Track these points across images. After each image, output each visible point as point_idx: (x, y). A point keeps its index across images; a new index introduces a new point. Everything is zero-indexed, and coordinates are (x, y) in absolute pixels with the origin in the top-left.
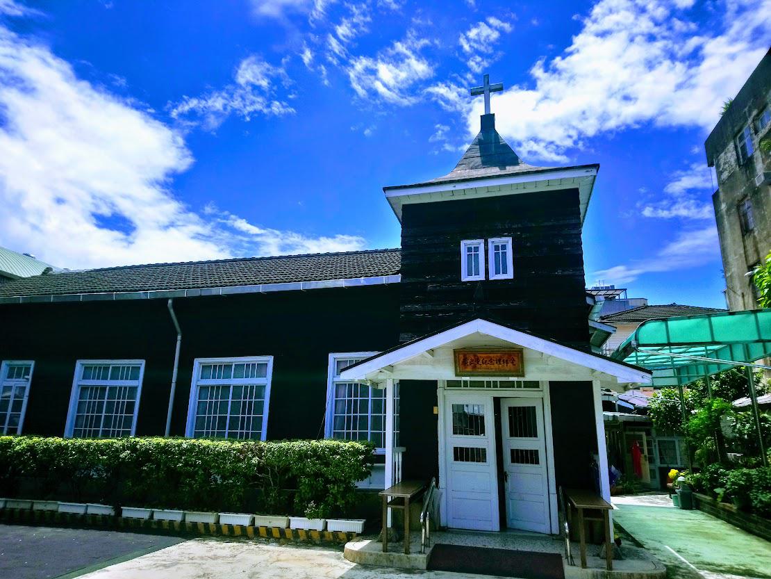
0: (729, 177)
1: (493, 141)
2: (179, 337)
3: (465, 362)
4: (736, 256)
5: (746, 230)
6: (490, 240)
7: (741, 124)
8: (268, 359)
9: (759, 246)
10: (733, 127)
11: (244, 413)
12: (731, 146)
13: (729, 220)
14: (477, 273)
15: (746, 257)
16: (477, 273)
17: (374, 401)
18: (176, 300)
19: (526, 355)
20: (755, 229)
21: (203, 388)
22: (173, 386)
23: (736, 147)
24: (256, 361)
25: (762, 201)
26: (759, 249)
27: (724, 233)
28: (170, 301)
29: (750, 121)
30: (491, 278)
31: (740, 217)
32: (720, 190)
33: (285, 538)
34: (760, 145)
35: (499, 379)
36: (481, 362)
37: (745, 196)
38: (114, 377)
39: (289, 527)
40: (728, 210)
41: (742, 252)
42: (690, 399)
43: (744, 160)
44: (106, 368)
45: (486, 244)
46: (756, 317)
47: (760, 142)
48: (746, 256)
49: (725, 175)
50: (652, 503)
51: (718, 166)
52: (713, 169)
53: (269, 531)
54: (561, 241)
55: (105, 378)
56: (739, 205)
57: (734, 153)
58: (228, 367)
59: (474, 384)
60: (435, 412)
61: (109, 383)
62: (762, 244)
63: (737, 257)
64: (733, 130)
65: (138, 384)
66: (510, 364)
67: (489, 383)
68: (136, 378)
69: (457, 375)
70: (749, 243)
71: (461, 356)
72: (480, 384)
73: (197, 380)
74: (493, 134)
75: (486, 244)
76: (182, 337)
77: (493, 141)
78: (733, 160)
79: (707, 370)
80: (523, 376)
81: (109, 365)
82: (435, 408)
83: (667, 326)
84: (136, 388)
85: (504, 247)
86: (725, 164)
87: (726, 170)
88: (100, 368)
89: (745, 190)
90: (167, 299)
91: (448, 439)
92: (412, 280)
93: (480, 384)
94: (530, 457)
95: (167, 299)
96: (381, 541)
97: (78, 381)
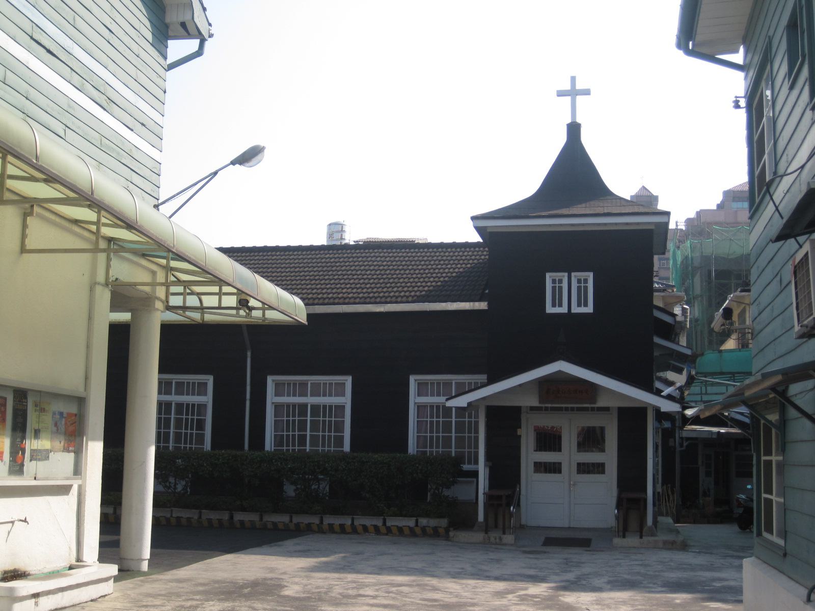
2: (249, 354)
6: (573, 274)
8: (208, 378)
14: (560, 305)
16: (560, 305)
17: (170, 414)
24: (328, 380)
30: (573, 311)
33: (391, 533)
35: (549, 405)
38: (179, 392)
39: (171, 516)
53: (400, 530)
58: (304, 385)
59: (553, 409)
61: (311, 400)
68: (343, 394)
69: (540, 403)
72: (560, 409)
73: (271, 398)
76: (252, 354)
81: (173, 379)
85: (586, 281)
91: (529, 455)
93: (560, 409)
94: (599, 468)
97: (414, 399)
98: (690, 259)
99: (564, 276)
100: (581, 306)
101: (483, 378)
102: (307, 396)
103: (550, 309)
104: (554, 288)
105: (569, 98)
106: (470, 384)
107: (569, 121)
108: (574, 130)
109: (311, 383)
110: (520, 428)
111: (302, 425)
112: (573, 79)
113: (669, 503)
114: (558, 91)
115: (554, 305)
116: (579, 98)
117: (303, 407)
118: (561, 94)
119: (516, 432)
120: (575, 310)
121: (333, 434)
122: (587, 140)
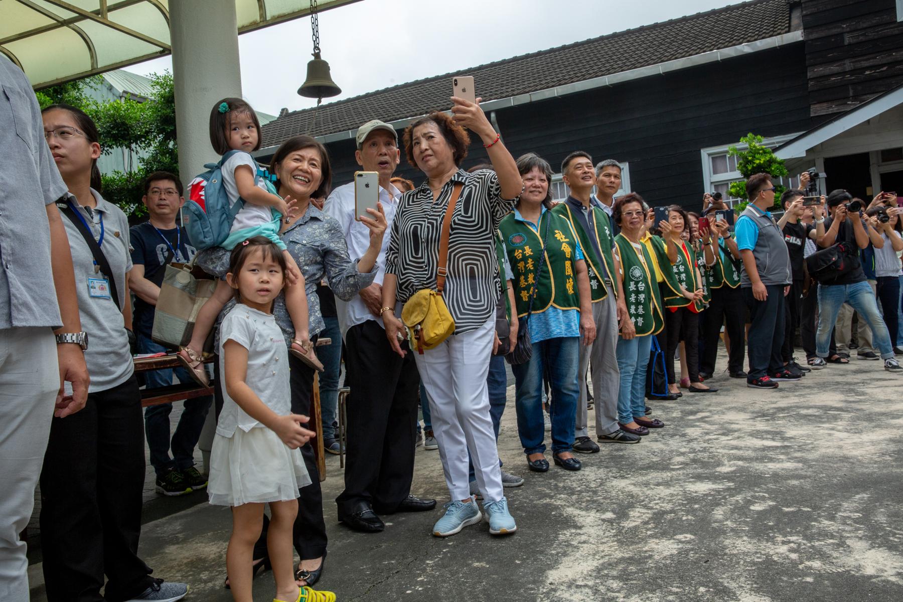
110: (871, 185)
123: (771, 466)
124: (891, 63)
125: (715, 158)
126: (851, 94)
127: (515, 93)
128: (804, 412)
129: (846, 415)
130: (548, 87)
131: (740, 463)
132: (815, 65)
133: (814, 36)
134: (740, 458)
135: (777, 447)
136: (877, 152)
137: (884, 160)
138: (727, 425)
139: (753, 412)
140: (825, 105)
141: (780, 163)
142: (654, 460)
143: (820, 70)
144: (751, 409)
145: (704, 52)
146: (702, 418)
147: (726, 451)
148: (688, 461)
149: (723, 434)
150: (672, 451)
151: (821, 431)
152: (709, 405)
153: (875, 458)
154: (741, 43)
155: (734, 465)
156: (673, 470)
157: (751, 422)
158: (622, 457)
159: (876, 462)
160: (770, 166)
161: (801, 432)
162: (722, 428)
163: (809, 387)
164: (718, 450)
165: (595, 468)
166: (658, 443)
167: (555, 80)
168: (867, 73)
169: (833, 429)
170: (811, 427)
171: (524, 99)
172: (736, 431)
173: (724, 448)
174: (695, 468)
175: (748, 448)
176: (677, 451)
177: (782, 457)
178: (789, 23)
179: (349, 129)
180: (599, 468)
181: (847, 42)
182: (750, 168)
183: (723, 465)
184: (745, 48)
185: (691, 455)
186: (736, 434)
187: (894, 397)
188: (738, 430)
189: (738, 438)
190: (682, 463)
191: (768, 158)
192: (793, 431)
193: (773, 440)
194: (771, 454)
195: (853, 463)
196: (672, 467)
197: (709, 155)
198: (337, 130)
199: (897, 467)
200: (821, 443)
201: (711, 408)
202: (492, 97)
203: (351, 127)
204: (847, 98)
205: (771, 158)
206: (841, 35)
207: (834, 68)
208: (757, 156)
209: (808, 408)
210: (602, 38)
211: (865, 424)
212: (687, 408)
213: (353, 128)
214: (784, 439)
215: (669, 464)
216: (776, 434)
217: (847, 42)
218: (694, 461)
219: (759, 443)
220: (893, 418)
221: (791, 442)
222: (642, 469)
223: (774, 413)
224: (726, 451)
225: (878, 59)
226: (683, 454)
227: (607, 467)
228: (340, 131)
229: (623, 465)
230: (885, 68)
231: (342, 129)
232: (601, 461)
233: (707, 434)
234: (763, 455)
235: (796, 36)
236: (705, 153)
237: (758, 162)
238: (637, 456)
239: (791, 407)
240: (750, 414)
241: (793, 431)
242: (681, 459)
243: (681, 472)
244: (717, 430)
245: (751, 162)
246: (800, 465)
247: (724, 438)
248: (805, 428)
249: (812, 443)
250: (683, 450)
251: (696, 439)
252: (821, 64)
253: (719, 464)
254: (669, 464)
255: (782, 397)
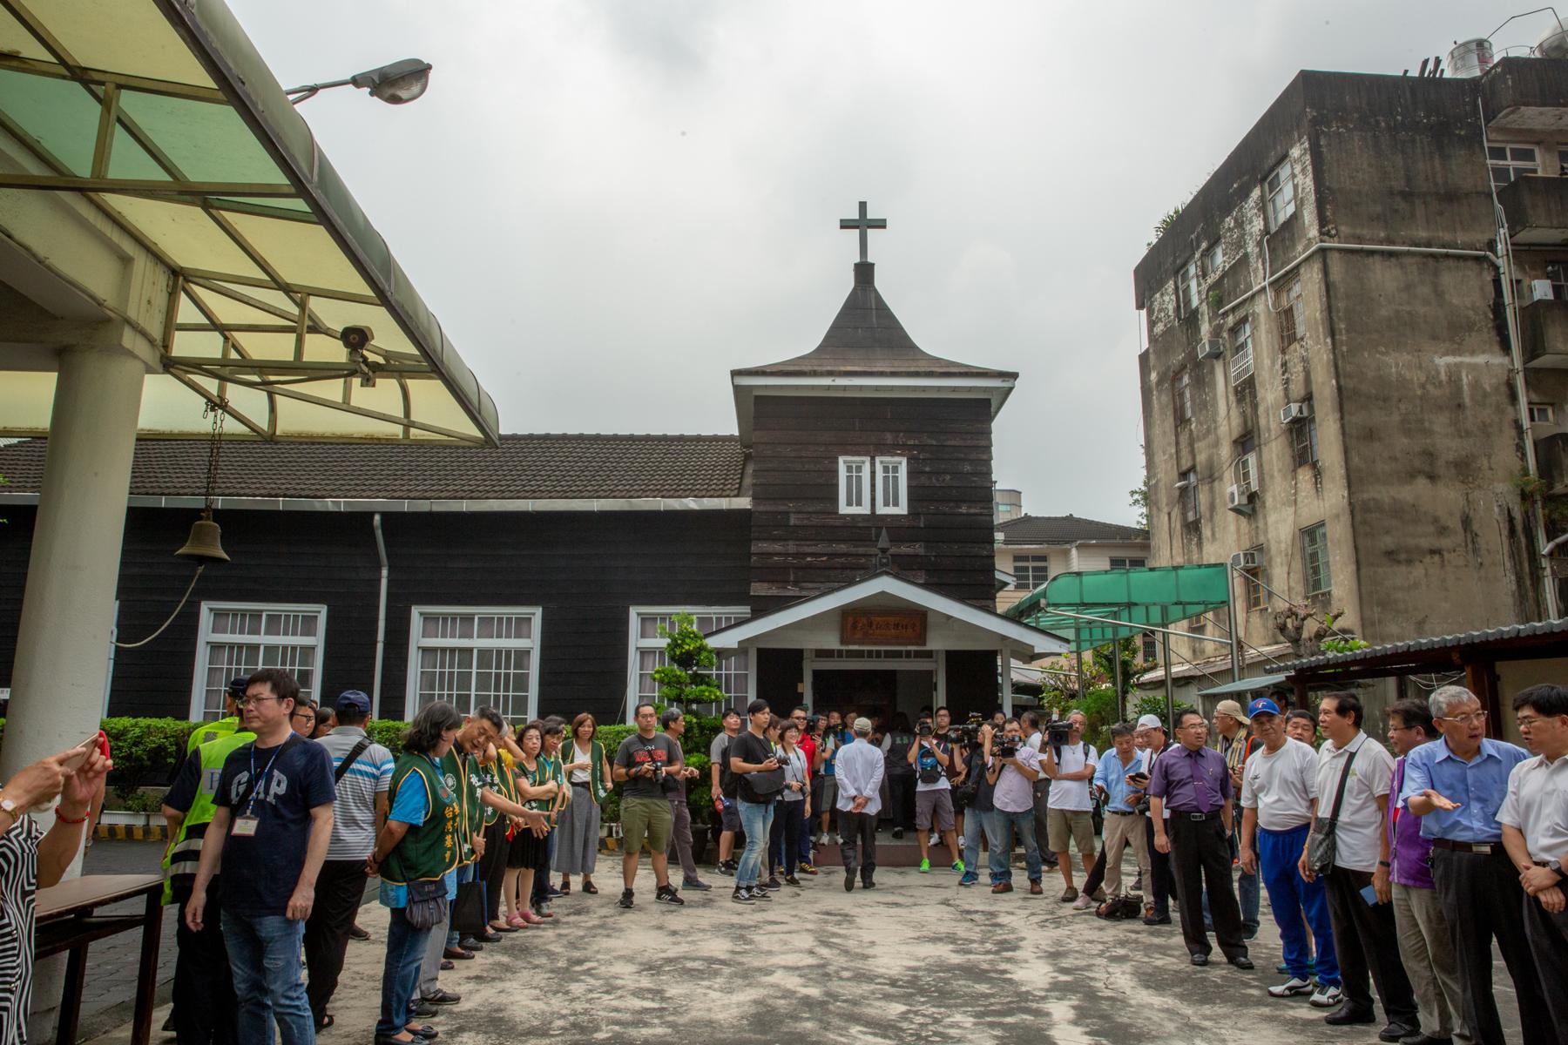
0: (1164, 333)
1: (874, 307)
2: (385, 572)
3: (854, 627)
4: (1164, 455)
5: (1181, 420)
6: (878, 459)
7: (1187, 255)
9: (1196, 446)
10: (1175, 259)
11: (497, 689)
12: (1171, 284)
13: (1159, 398)
14: (859, 503)
15: (1178, 459)
16: (859, 503)
18: (386, 516)
19: (931, 619)
20: (1193, 419)
21: (216, 647)
22: (380, 647)
23: (1177, 288)
25: (1204, 379)
26: (1196, 451)
27: (1151, 416)
28: (377, 518)
29: (1197, 255)
31: (1174, 395)
32: (1151, 351)
34: (1207, 295)
36: (874, 627)
37: (1183, 367)
40: (1160, 382)
41: (1173, 451)
42: (602, 794)
43: (1185, 313)
44: (256, 616)
45: (873, 464)
46: (1177, 575)
47: (1208, 291)
48: (1177, 458)
49: (1159, 328)
50: (1360, 240)
51: (1150, 313)
52: (1144, 312)
54: (968, 468)
55: (255, 631)
56: (1177, 377)
57: (1174, 297)
60: (799, 691)
61: (263, 639)
62: (1200, 444)
63: (1166, 457)
64: (1174, 261)
65: (318, 641)
66: (910, 630)
67: (870, 652)
69: (843, 642)
70: (1184, 439)
71: (850, 619)
73: (418, 637)
74: (873, 295)
75: (873, 464)
77: (874, 307)
78: (1171, 307)
79: (1115, 633)
80: (925, 644)
82: (800, 685)
83: (1081, 582)
84: (313, 648)
86: (1160, 310)
87: (1160, 320)
88: (296, 617)
89: (1183, 358)
90: (371, 514)
92: (769, 508)
95: (371, 514)
96: (1425, 513)
98: (975, 443)
99: (863, 462)
100: (888, 505)
101: (745, 610)
102: (259, 634)
103: (844, 509)
104: (849, 478)
105: (857, 231)
106: (728, 619)
107: (858, 260)
108: (864, 272)
109: (268, 615)
110: (802, 681)
111: (464, 680)
112: (863, 206)
113: (611, 764)
114: (841, 221)
115: (849, 504)
116: (872, 234)
117: (254, 648)
118: (846, 225)
119: (796, 688)
120: (882, 510)
121: (511, 694)
122: (881, 283)
123: (645, 1032)
124: (831, 554)
125: (645, 619)
126: (792, 578)
127: (412, 495)
128: (689, 965)
129: (727, 970)
130: (455, 498)
131: (617, 1028)
132: (759, 539)
133: (761, 508)
134: (617, 1022)
135: (654, 1009)
136: (811, 650)
137: (816, 656)
138: (612, 981)
139: (641, 964)
140: (766, 585)
141: (710, 652)
142: (535, 1024)
143: (764, 546)
144: (640, 959)
145: (647, 497)
146: (589, 969)
147: (606, 1014)
148: (568, 1025)
149: (607, 992)
150: (553, 1013)
151: (699, 990)
152: (598, 952)
153: (735, 1022)
154: (687, 497)
155: (611, 1030)
156: (553, 1036)
157: (636, 977)
158: (501, 1019)
159: (733, 1027)
160: (699, 654)
161: (680, 991)
162: (608, 984)
163: (703, 930)
164: (599, 1013)
165: (472, 1034)
166: (540, 1002)
167: (465, 488)
168: (809, 559)
169: (709, 988)
170: (691, 984)
171: (424, 506)
172: (619, 988)
173: (604, 1009)
174: (574, 1034)
175: (627, 1010)
176: (558, 1013)
177: (656, 1021)
178: (740, 483)
179: (163, 494)
180: (478, 1033)
181: (792, 522)
182: (678, 653)
183: (601, 1030)
184: (691, 504)
185: (572, 1018)
186: (619, 993)
187: (776, 948)
188: (623, 987)
189: (621, 997)
190: (562, 1028)
191: (698, 645)
192: (674, 990)
193: (653, 1000)
194: (646, 1018)
195: (715, 1028)
196: (552, 1032)
197: (639, 614)
198: (143, 490)
199: (750, 1031)
200: (697, 1005)
201: (599, 957)
202: (380, 494)
203: (166, 491)
204: (787, 582)
205: (701, 645)
206: (787, 513)
207: (777, 547)
208: (688, 641)
209: (694, 959)
210: (531, 437)
211: (740, 981)
212: (574, 954)
213: (169, 494)
214: (663, 999)
215: (550, 1029)
216: (658, 993)
217: (792, 522)
218: (574, 1025)
219: (638, 1004)
220: (766, 975)
221: (668, 1004)
222: (522, 1035)
223: (661, 966)
224: (606, 1014)
225: (819, 548)
226: (564, 1017)
227: (486, 1033)
228: (147, 494)
229: (502, 1030)
230: (824, 559)
231: (151, 491)
232: (480, 1025)
233: (591, 991)
234: (640, 1018)
235: (744, 503)
236: (633, 612)
237: (687, 647)
238: (517, 1019)
239: (679, 958)
240: (637, 966)
241: (674, 990)
242: (560, 1023)
243: (559, 1039)
244: (601, 986)
245: (680, 646)
246: (670, 1030)
247: (606, 997)
248: (686, 985)
249: (686, 1005)
250: (564, 1012)
251: (579, 998)
252: (765, 540)
253: (597, 1029)
254: (550, 1029)
255: (674, 944)
